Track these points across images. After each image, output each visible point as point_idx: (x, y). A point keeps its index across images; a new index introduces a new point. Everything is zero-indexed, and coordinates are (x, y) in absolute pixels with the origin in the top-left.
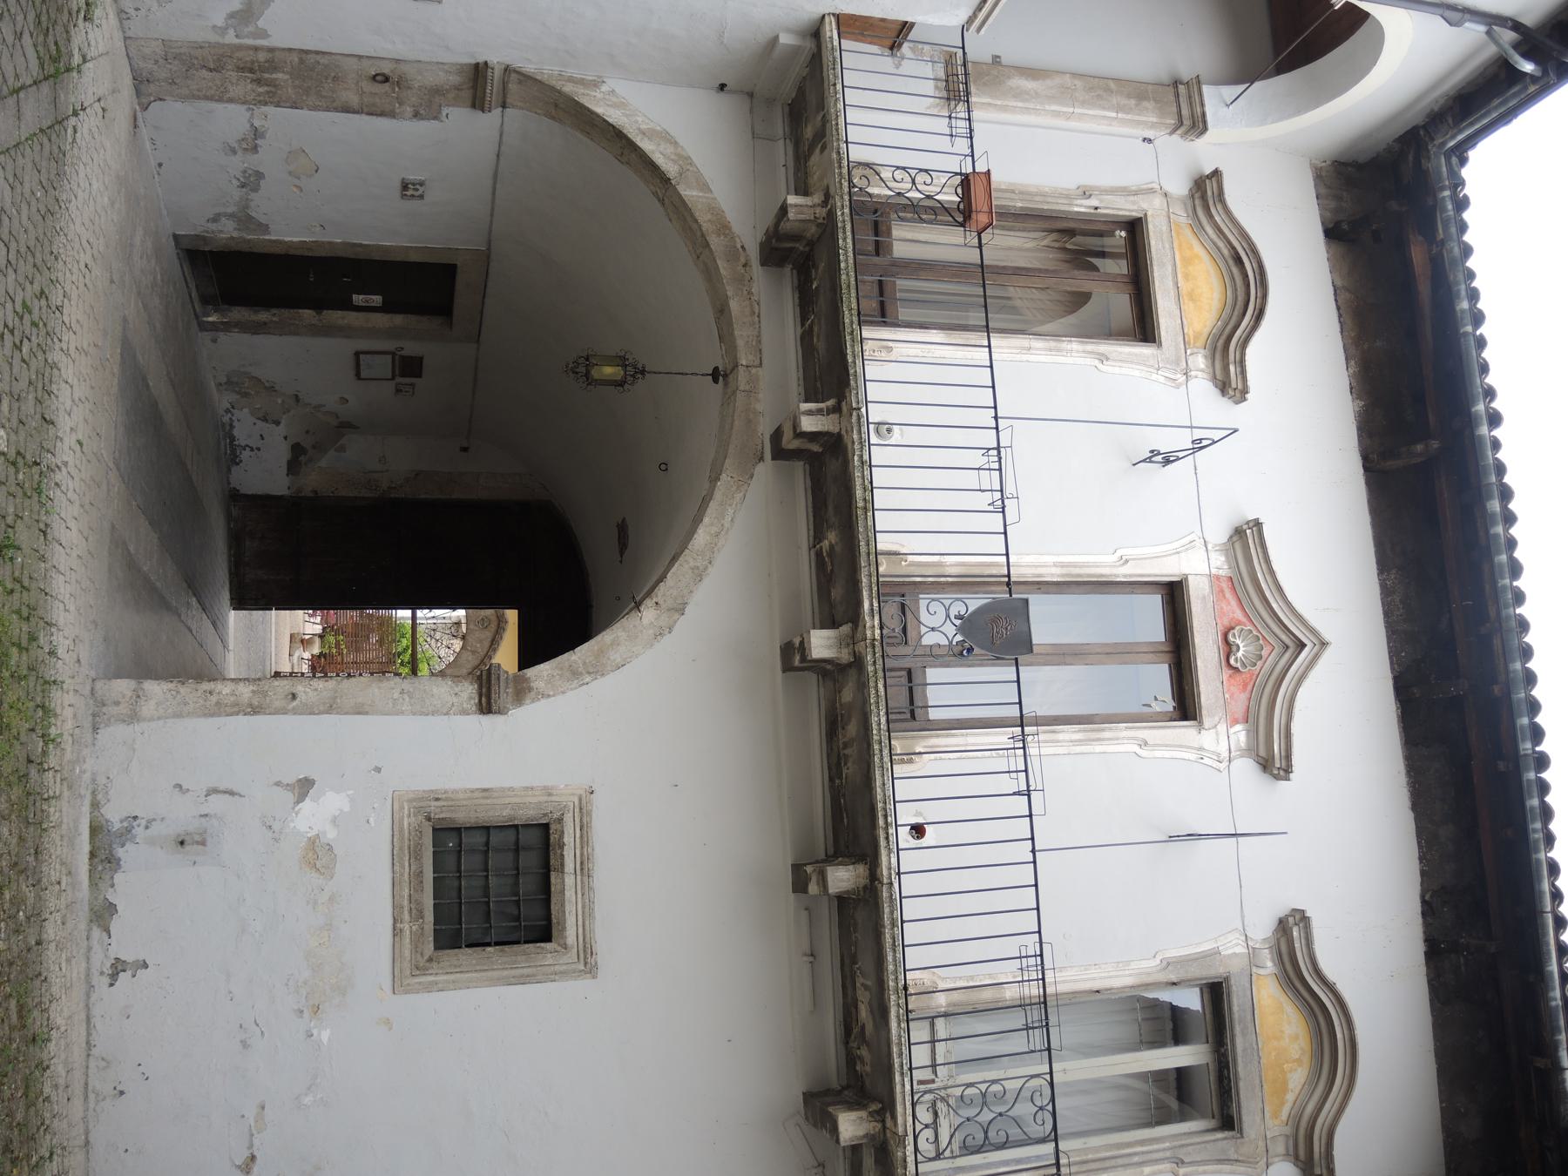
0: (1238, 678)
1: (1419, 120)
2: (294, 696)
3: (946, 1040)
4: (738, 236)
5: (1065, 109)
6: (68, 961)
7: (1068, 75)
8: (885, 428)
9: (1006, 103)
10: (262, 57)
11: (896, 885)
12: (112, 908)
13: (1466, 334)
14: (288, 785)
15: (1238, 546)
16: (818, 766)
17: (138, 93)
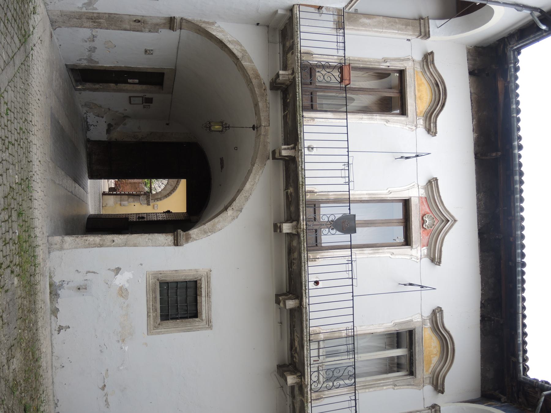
0: (426, 231)
1: (506, 36)
2: (113, 241)
3: (323, 348)
4: (262, 79)
5: (380, 30)
6: (45, 330)
7: (381, 17)
8: (310, 148)
9: (358, 28)
10: (95, 15)
11: (308, 308)
12: (57, 310)
13: (514, 117)
14: (112, 270)
15: (429, 187)
16: (285, 264)
17: (52, 25)
